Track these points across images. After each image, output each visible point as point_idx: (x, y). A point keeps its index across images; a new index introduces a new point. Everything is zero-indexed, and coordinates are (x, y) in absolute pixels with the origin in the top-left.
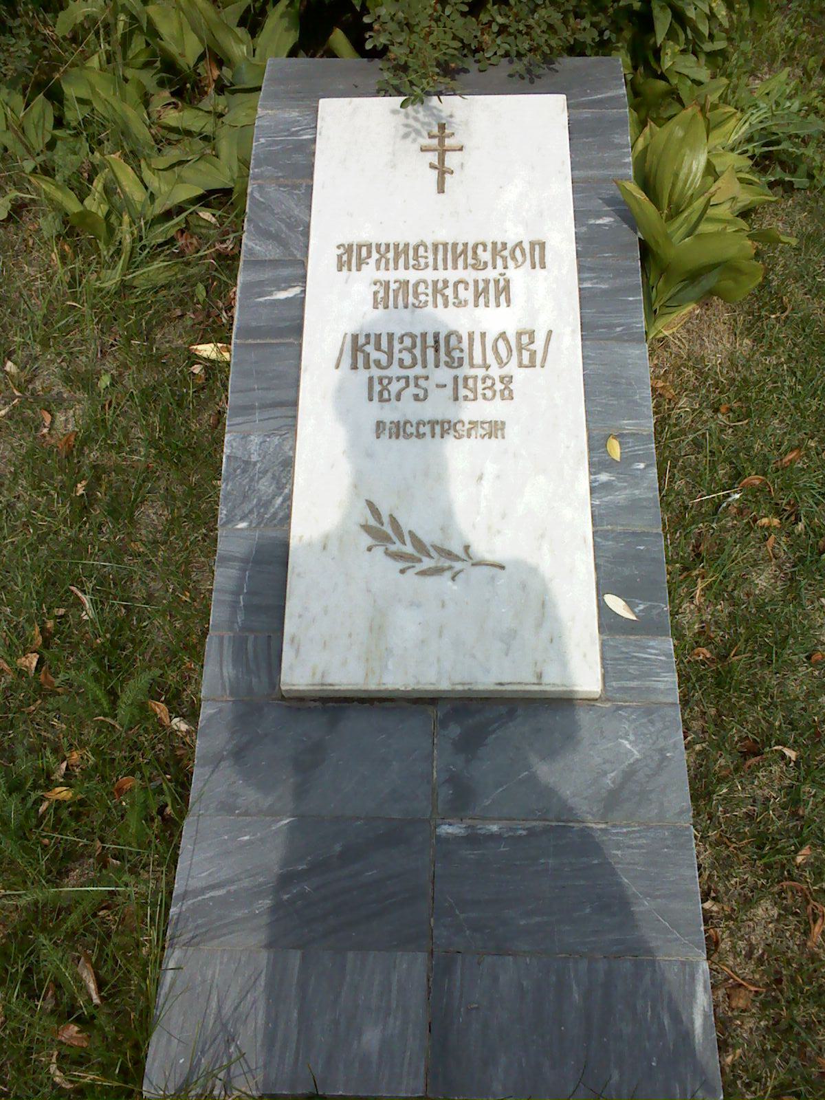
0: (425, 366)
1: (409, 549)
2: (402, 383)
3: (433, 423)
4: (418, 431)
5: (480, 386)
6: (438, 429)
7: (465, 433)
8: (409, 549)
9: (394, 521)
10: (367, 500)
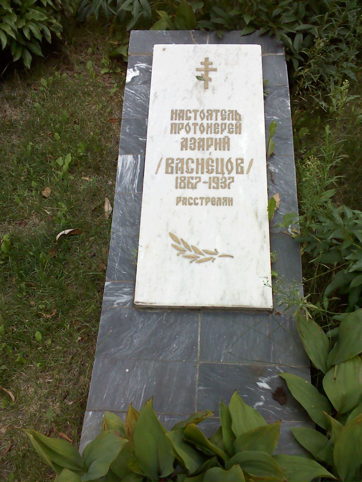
0: (197, 173)
3: (202, 198)
5: (189, 143)
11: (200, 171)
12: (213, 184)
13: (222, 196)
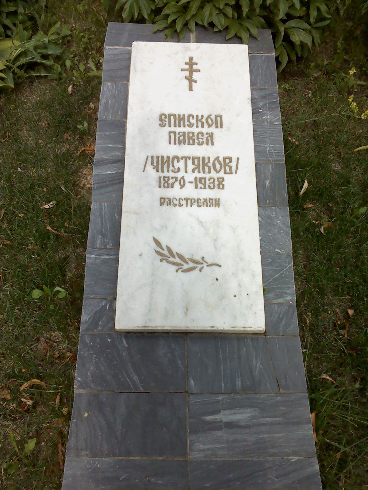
2: (174, 180)
3: (187, 200)
4: (179, 202)
5: (208, 182)
6: (189, 202)
7: (202, 204)
9: (169, 249)
12: (200, 185)
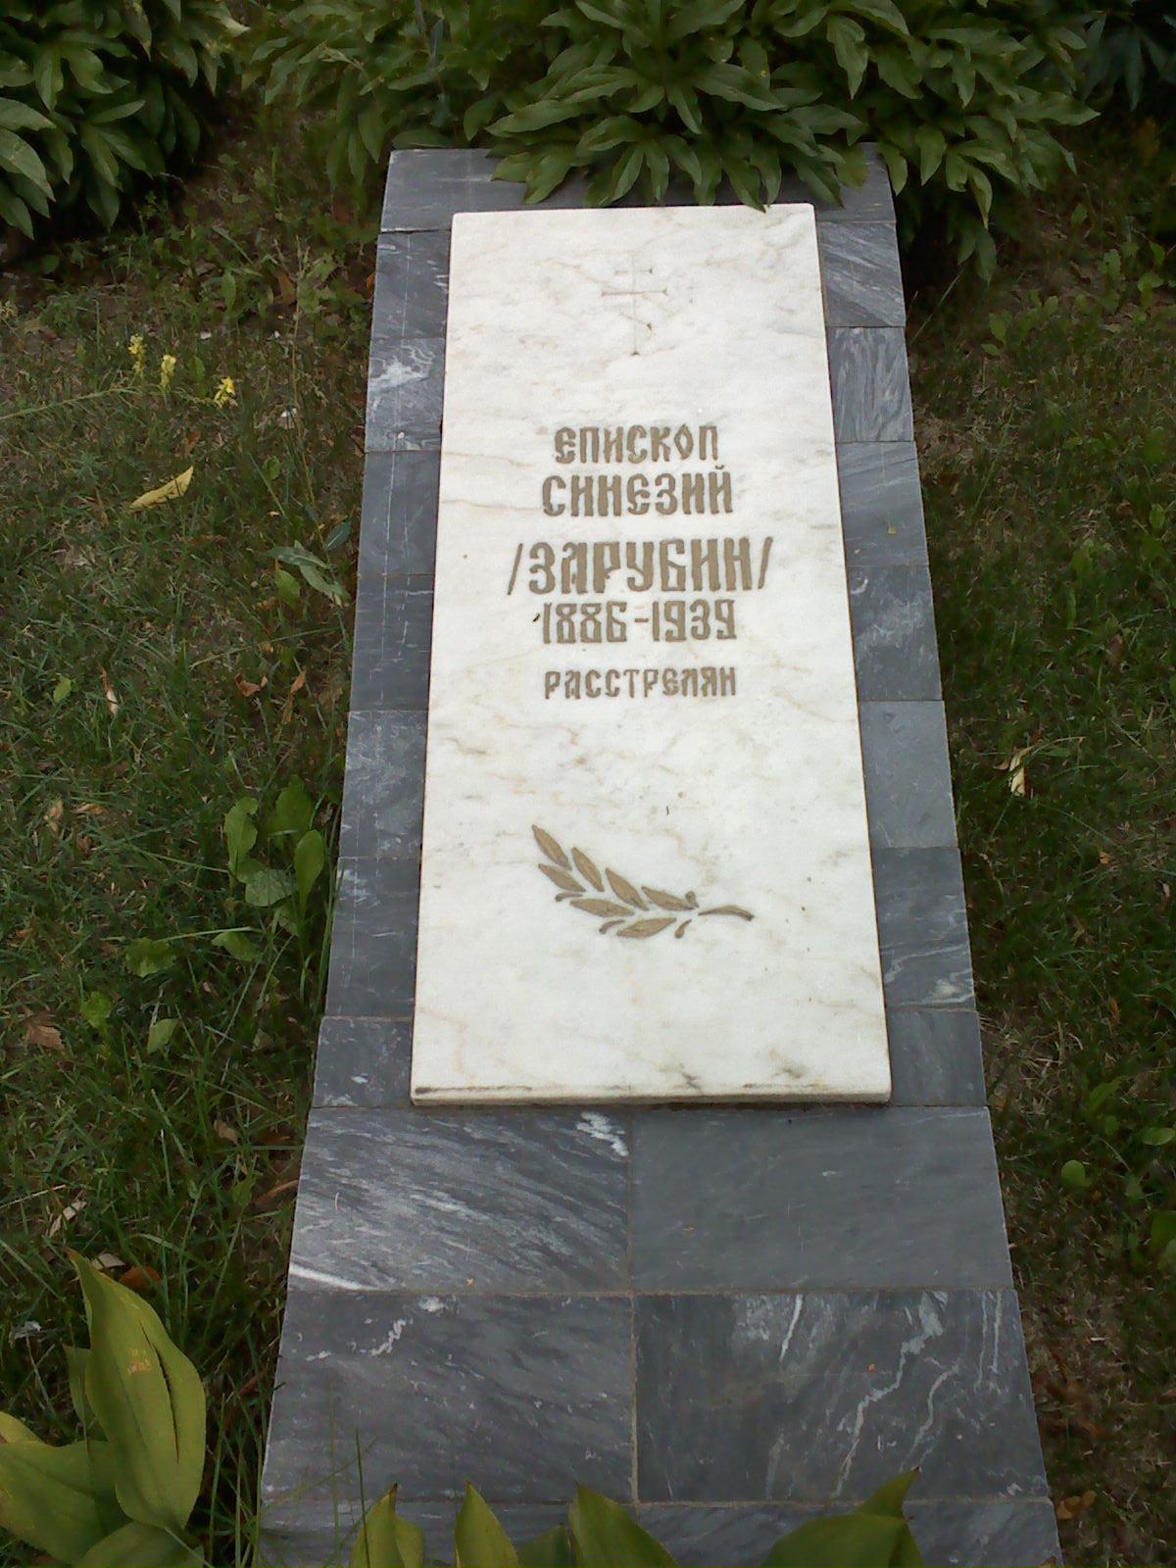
0: (698, 588)
1: (609, 895)
8: (609, 895)
10: (534, 828)
11: (706, 583)
12: (665, 626)
13: (690, 663)
